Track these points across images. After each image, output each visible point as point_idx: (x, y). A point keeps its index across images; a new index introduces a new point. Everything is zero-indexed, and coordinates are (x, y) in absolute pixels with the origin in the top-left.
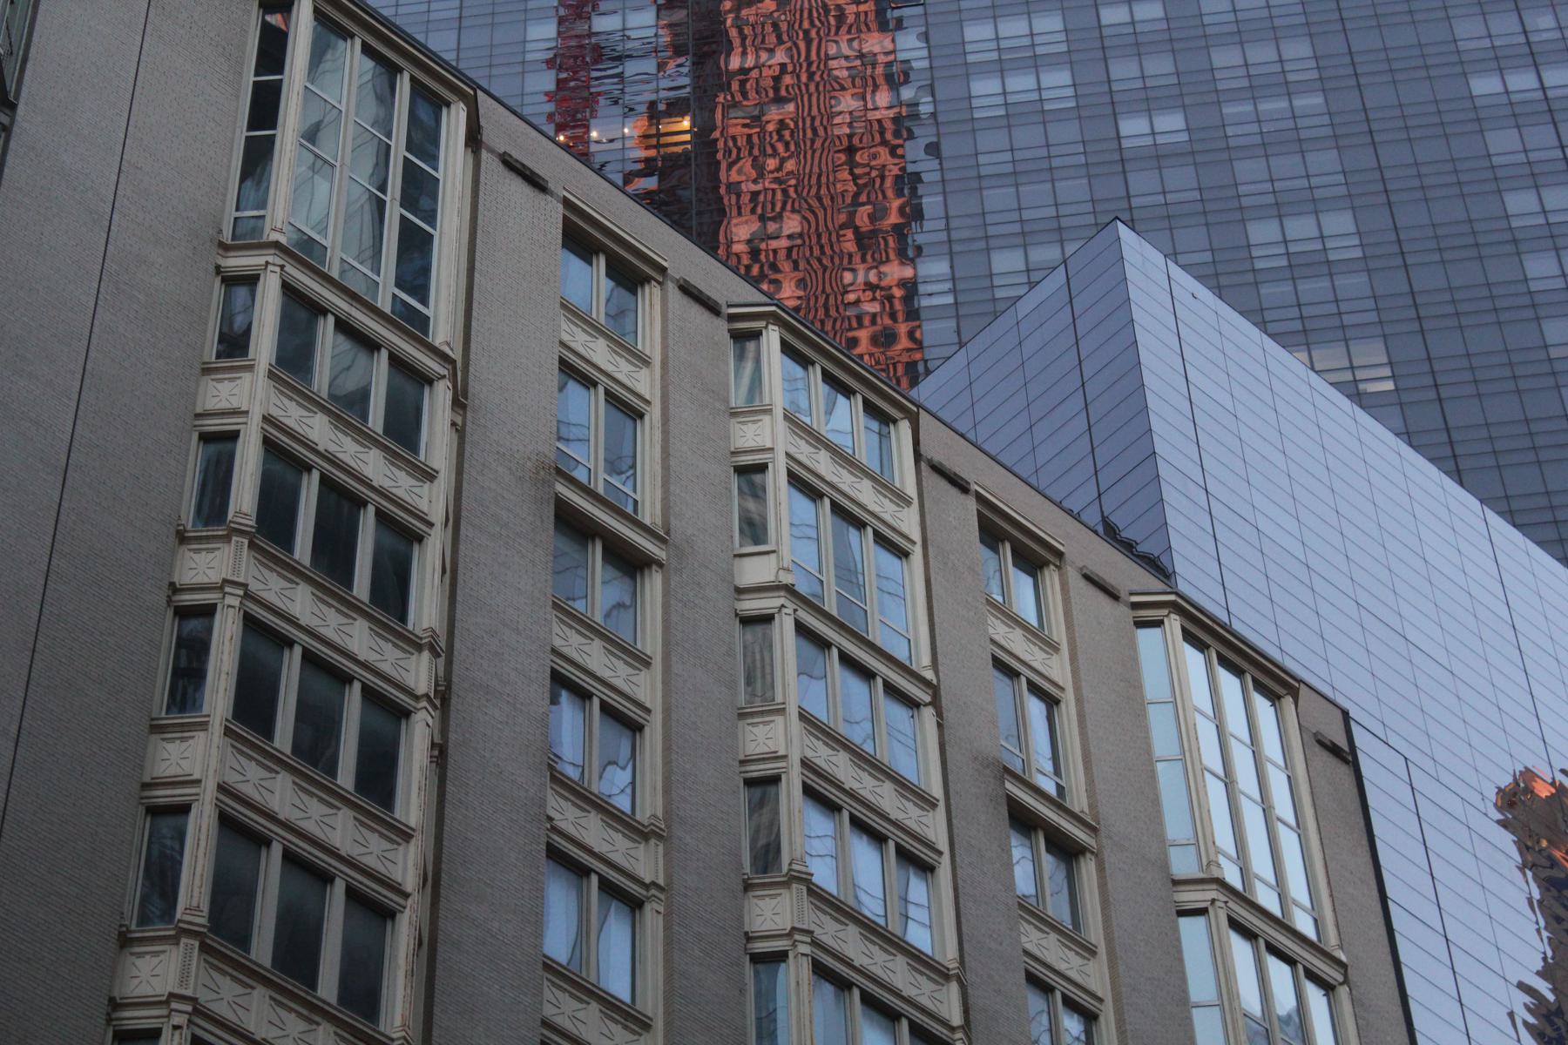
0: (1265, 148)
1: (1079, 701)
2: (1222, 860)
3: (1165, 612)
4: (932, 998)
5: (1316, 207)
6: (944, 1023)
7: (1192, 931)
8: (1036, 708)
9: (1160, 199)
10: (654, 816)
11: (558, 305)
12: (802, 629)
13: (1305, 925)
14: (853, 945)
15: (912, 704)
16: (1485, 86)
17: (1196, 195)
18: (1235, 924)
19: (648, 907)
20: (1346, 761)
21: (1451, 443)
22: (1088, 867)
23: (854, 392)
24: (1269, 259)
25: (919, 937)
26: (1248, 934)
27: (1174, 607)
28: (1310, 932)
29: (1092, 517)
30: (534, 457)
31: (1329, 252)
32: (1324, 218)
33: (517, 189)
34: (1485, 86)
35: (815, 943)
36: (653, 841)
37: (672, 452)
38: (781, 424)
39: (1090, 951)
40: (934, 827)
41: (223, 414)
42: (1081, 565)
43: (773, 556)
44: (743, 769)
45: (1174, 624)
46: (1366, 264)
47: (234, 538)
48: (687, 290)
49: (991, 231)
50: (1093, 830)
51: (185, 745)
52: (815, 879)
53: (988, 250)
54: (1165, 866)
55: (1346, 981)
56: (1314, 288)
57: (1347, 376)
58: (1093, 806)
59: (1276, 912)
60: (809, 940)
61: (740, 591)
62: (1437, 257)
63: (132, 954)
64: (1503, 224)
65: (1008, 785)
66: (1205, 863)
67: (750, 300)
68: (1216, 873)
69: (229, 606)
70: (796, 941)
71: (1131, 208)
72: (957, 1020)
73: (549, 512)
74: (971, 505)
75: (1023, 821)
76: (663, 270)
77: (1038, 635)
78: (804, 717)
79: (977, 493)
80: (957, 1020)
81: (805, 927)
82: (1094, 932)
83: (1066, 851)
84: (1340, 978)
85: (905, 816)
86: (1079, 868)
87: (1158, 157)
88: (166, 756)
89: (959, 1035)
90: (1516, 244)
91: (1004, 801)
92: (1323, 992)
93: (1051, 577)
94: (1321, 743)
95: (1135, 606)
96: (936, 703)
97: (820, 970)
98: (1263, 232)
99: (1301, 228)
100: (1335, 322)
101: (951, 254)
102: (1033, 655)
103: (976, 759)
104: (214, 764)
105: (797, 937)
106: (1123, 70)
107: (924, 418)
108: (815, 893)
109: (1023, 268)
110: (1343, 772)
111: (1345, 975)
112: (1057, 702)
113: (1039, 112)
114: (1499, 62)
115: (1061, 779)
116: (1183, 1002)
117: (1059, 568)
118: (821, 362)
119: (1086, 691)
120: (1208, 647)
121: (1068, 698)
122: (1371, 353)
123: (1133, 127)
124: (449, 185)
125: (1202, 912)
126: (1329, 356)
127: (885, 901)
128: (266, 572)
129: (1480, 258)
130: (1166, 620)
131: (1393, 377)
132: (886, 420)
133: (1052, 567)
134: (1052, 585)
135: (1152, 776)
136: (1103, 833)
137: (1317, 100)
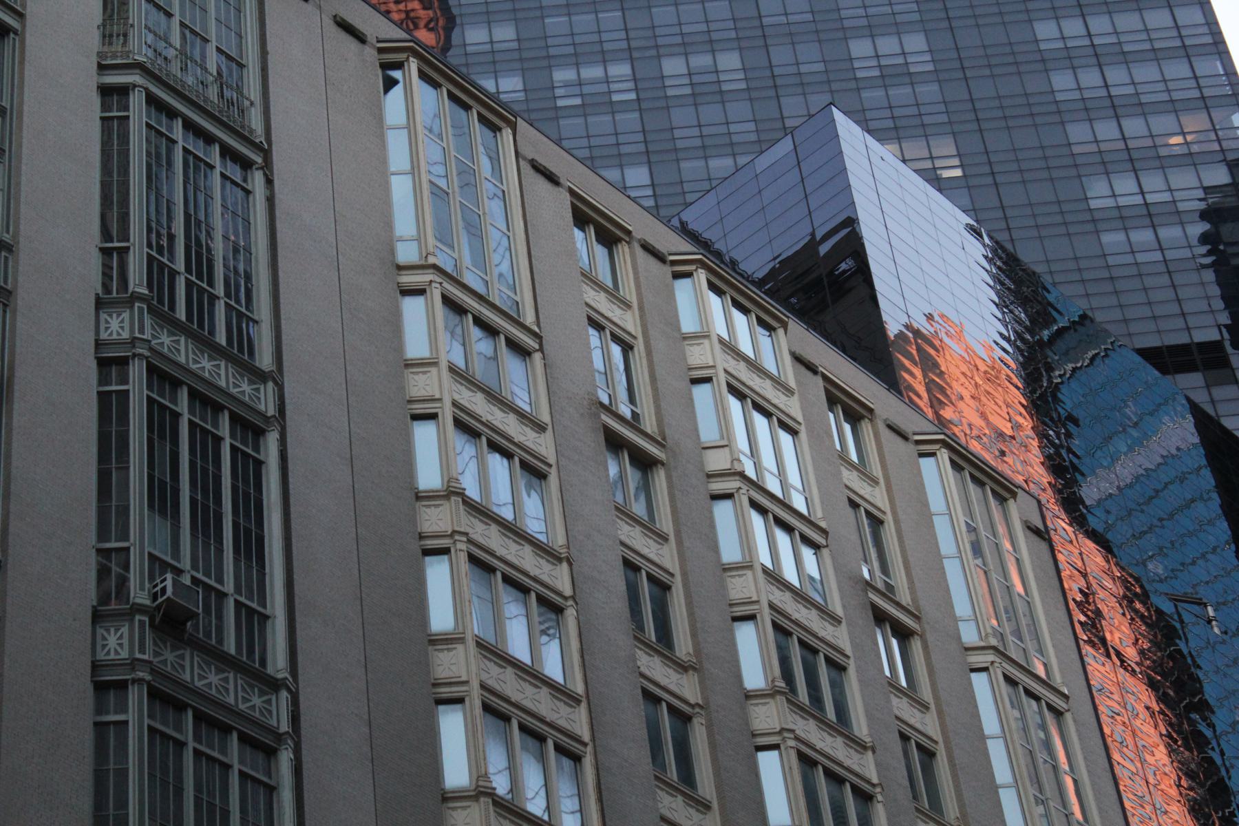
1: (897, 521)
2: (742, 458)
3: (937, 447)
4: (550, 575)
6: (868, 782)
8: (616, 350)
9: (783, 19)
10: (689, 653)
11: (579, 275)
12: (152, 100)
13: (799, 503)
14: (493, 539)
17: (809, 17)
18: (754, 504)
19: (695, 720)
20: (1044, 539)
21: (1006, 218)
22: (660, 478)
23: (724, 293)
24: (865, 70)
25: (534, 526)
26: (762, 511)
27: (944, 444)
28: (803, 510)
29: (675, 222)
30: (586, 397)
31: (910, 66)
32: (905, 38)
33: (542, 184)
35: (470, 541)
36: (691, 672)
37: (658, 376)
38: (717, 346)
39: (924, 707)
40: (543, 445)
41: (424, 400)
42: (884, 418)
43: (727, 449)
44: (409, 407)
45: (944, 455)
46: (937, 76)
47: (137, 305)
48: (647, 248)
49: (660, 41)
50: (917, 618)
51: (451, 654)
52: (467, 493)
53: (659, 57)
54: (392, 252)
55: (541, 350)
56: (900, 94)
57: (928, 164)
58: (914, 600)
59: (779, 494)
60: (465, 539)
62: (987, 72)
63: (449, 808)
64: (1033, 47)
65: (871, 595)
66: (983, 635)
67: (927, 430)
68: (738, 468)
69: (460, 550)
70: (784, 738)
71: (762, 26)
72: (568, 592)
75: (615, 443)
76: (629, 233)
77: (613, 293)
78: (453, 369)
79: (570, 188)
80: (568, 592)
81: (462, 530)
82: (926, 694)
83: (644, 463)
84: (537, 347)
85: (525, 438)
86: (911, 647)
88: (440, 662)
89: (570, 602)
90: (1045, 63)
91: (869, 607)
92: (813, 551)
93: (866, 427)
94: (1029, 528)
95: (918, 442)
97: (473, 559)
98: (860, 48)
99: (888, 45)
100: (917, 121)
101: (632, 59)
103: (850, 578)
104: (474, 668)
105: (457, 537)
107: (521, 124)
108: (468, 503)
109: (686, 72)
110: (1044, 546)
111: (541, 345)
112: (631, 348)
115: (636, 407)
117: (871, 420)
119: (902, 516)
120: (963, 469)
121: (640, 346)
122: (945, 147)
124: (512, 193)
126: (916, 149)
127: (514, 504)
128: (472, 519)
129: (1019, 73)
130: (695, 274)
131: (962, 166)
132: (495, 129)
133: (867, 420)
134: (869, 435)
136: (924, 619)
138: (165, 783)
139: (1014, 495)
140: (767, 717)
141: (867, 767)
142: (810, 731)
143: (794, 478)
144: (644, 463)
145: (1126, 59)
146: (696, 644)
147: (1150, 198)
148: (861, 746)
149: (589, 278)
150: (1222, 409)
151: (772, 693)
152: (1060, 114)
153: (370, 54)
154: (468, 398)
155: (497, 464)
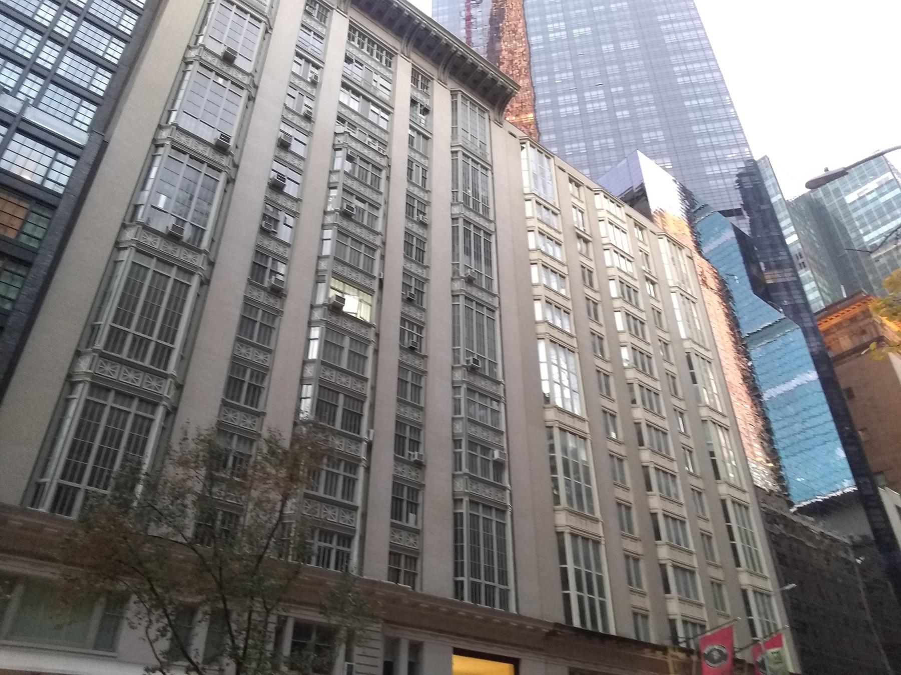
0: (559, 61)
5: (655, 130)
7: (606, 253)
8: (580, 214)
12: (464, 154)
15: (487, 169)
16: (687, 103)
18: (615, 252)
22: (656, 286)
34: (687, 103)
45: (602, 194)
46: (665, 142)
56: (655, 147)
61: (603, 244)
73: (575, 235)
74: (567, 175)
82: (659, 298)
83: (586, 241)
87: (624, 120)
93: (644, 232)
96: (492, 170)
99: (652, 134)
102: (579, 204)
106: (616, 102)
108: (542, 252)
113: (600, 111)
116: (673, 309)
118: (545, 153)
121: (585, 212)
122: (667, 160)
123: (619, 114)
125: (530, 200)
126: (660, 161)
135: (664, 267)
140: (618, 304)
142: (628, 307)
144: (586, 241)
145: (716, 135)
148: (641, 311)
153: (517, 141)
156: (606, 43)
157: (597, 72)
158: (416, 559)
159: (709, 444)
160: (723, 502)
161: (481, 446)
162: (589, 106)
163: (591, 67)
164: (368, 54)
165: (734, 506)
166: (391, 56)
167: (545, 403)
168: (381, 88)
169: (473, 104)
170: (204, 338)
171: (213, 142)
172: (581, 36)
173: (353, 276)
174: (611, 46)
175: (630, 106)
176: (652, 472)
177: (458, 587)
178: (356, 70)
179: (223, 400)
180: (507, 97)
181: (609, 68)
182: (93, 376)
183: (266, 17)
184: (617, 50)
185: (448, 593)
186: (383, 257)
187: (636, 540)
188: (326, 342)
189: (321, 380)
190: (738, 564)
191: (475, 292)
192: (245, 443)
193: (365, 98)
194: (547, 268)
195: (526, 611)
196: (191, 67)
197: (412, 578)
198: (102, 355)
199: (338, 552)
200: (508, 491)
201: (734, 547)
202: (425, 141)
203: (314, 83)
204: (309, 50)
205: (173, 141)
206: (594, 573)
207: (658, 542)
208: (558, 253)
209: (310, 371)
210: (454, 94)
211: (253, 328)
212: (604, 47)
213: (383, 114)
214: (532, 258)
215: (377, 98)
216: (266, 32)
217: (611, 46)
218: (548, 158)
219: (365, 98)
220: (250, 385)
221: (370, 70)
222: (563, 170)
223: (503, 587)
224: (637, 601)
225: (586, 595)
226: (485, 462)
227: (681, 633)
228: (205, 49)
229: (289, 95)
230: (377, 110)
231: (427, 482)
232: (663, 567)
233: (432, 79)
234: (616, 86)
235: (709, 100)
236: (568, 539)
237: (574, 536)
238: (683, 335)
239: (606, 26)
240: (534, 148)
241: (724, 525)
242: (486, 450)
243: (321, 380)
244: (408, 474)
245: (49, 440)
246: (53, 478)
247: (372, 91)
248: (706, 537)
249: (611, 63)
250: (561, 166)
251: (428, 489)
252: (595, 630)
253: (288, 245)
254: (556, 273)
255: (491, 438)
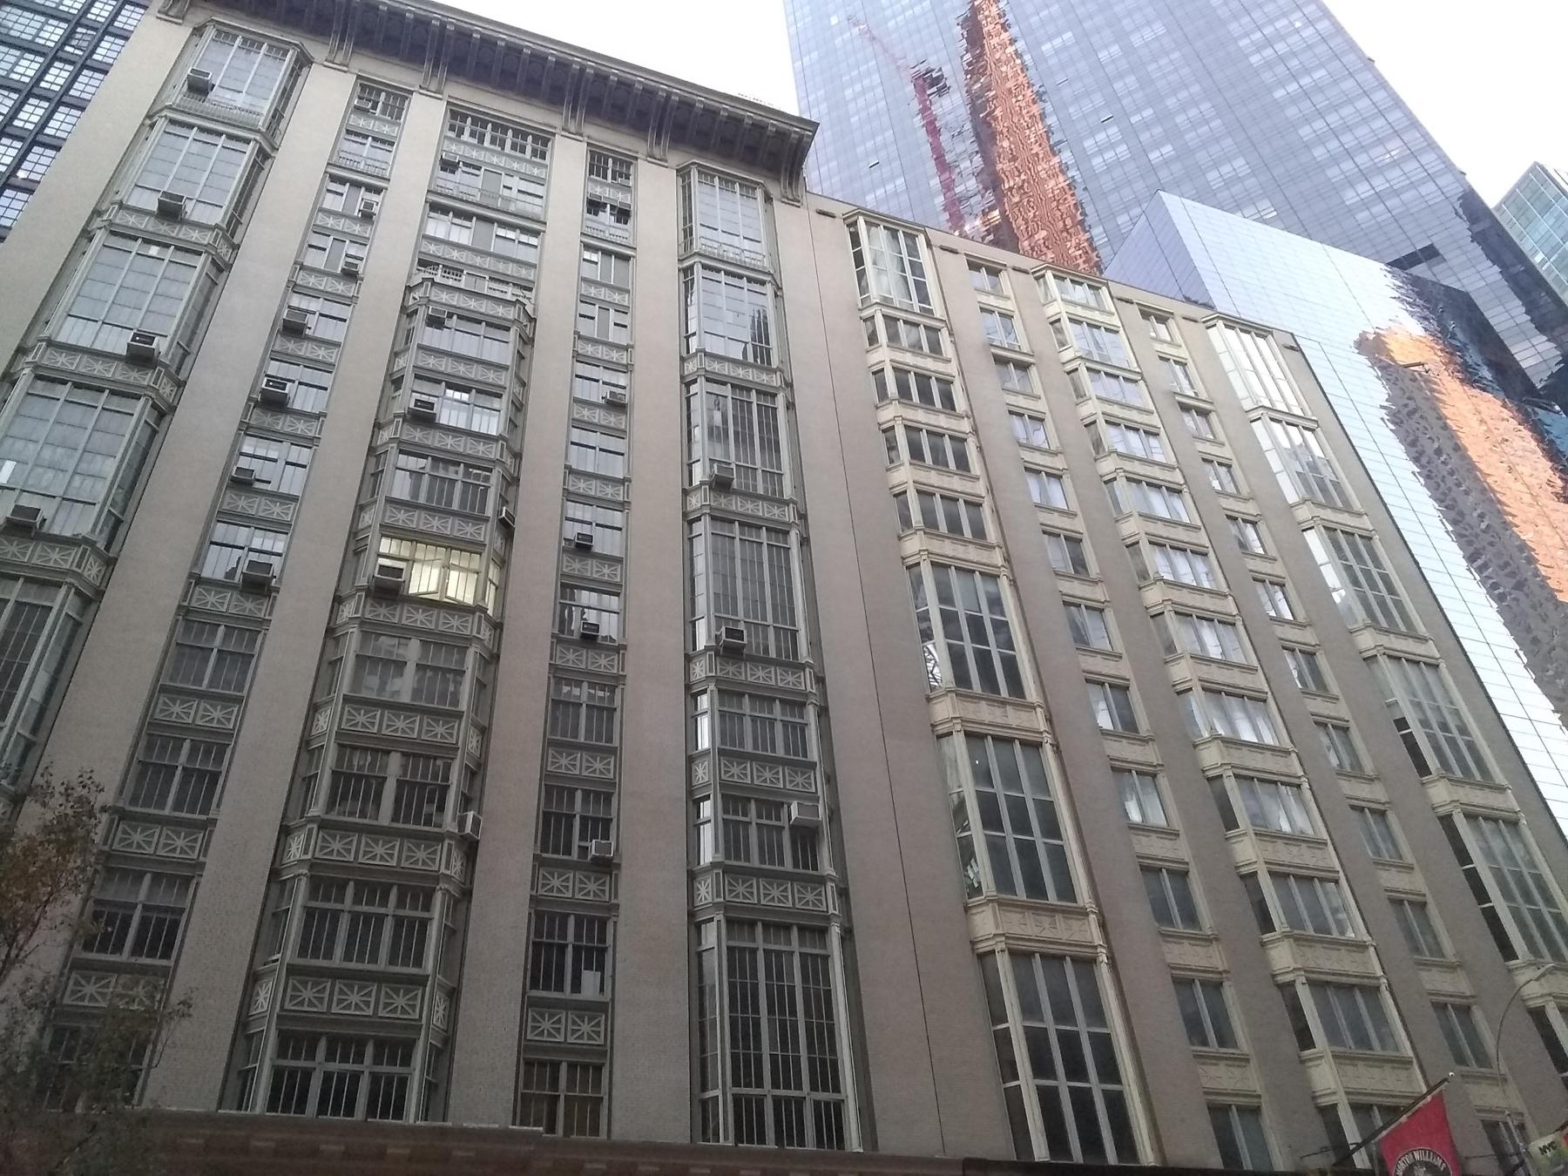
12: (1088, 369)
22: (1213, 417)
34: (1279, 94)
45: (1220, 323)
46: (1253, 174)
56: (1236, 189)
75: (1185, 408)
83: (1204, 413)
90: (1307, 147)
93: (1171, 322)
97: (1129, 479)
98: (1212, 175)
106: (1145, 137)
108: (1120, 455)
110: (1298, 354)
113: (1119, 163)
114: (1282, 84)
122: (1265, 204)
123: (1154, 156)
126: (1250, 210)
137: (1219, 121)
138: (780, 568)
139: (1272, 333)
140: (1304, 513)
141: (1366, 523)
142: (1328, 514)
143: (1292, 400)
144: (1023, 367)
145: (1349, 128)
146: (1250, 486)
147: (1377, 190)
148: (1360, 515)
149: (1157, 340)
150: (1465, 282)
151: (1304, 501)
152: (1321, 167)
153: (839, 221)
154: (1109, 409)
155: (1131, 435)
156: (1106, 47)
157: (1098, 100)
158: (598, 1069)
159: (1389, 705)
160: (1447, 821)
161: (756, 800)
162: (1097, 161)
163: (1088, 94)
164: (475, 141)
165: (1478, 830)
166: (545, 142)
167: (1421, 776)
168: (521, 196)
169: (728, 181)
170: (81, 699)
171: (122, 350)
172: (1057, 52)
173: (435, 524)
174: (1115, 49)
175: (1173, 135)
176: (1230, 784)
177: (704, 1111)
178: (467, 179)
179: (535, 857)
180: (795, 153)
181: (1118, 86)
182: (313, 865)
183: (769, 274)
184: (1129, 50)
185: (675, 1128)
186: (805, 541)
187: (1208, 940)
188: (723, 714)
189: (724, 785)
190: (1507, 951)
191: (736, 505)
192: (171, 886)
193: (481, 218)
194: (1139, 482)
195: (893, 1141)
196: (694, 389)
197: (590, 1110)
198: (324, 825)
199: (777, 1101)
200: (1372, 949)
201: (1491, 917)
202: (622, 264)
203: (367, 217)
204: (361, 167)
205: (400, 442)
206: (1083, 1028)
207: (1267, 937)
208: (1160, 451)
209: (702, 773)
210: (683, 173)
211: (577, 717)
212: (1103, 55)
213: (524, 238)
214: (1301, 519)
215: (516, 215)
216: (776, 296)
217: (1115, 49)
218: (1264, 337)
219: (481, 218)
220: (584, 819)
221: (495, 172)
222: (1128, 301)
223: (822, 1096)
224: (1223, 1078)
225: (1063, 1085)
226: (770, 834)
227: (1352, 1135)
228: (706, 354)
229: (581, 316)
230: (511, 235)
231: (622, 900)
232: (1287, 989)
233: (636, 158)
234: (1139, 110)
235: (1320, 74)
236: (1003, 963)
237: (1317, 985)
238: (1292, 497)
239: (1099, 20)
240: (1081, 284)
241: (1457, 873)
242: (772, 805)
243: (724, 785)
244: (572, 888)
245: (696, 1027)
246: (721, 1092)
247: (499, 204)
248: (1408, 907)
249: (1121, 76)
250: (945, 244)
251: (624, 914)
252: (1094, 1162)
253: (619, 560)
254: (1159, 487)
255: (781, 780)
